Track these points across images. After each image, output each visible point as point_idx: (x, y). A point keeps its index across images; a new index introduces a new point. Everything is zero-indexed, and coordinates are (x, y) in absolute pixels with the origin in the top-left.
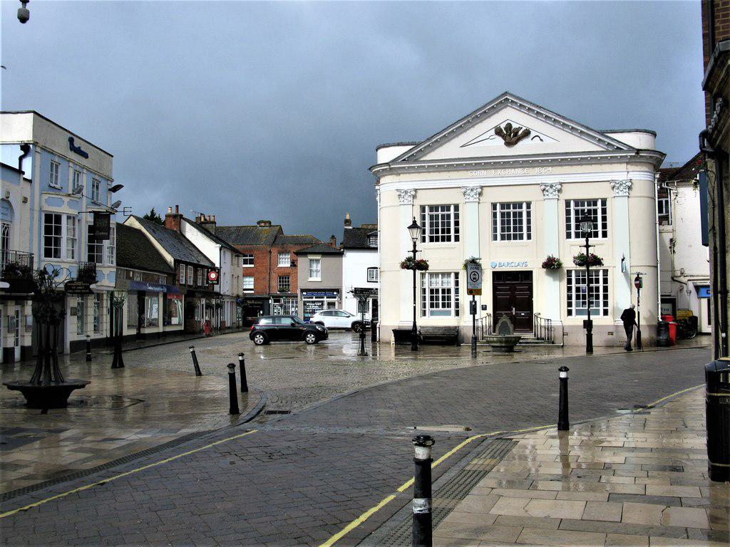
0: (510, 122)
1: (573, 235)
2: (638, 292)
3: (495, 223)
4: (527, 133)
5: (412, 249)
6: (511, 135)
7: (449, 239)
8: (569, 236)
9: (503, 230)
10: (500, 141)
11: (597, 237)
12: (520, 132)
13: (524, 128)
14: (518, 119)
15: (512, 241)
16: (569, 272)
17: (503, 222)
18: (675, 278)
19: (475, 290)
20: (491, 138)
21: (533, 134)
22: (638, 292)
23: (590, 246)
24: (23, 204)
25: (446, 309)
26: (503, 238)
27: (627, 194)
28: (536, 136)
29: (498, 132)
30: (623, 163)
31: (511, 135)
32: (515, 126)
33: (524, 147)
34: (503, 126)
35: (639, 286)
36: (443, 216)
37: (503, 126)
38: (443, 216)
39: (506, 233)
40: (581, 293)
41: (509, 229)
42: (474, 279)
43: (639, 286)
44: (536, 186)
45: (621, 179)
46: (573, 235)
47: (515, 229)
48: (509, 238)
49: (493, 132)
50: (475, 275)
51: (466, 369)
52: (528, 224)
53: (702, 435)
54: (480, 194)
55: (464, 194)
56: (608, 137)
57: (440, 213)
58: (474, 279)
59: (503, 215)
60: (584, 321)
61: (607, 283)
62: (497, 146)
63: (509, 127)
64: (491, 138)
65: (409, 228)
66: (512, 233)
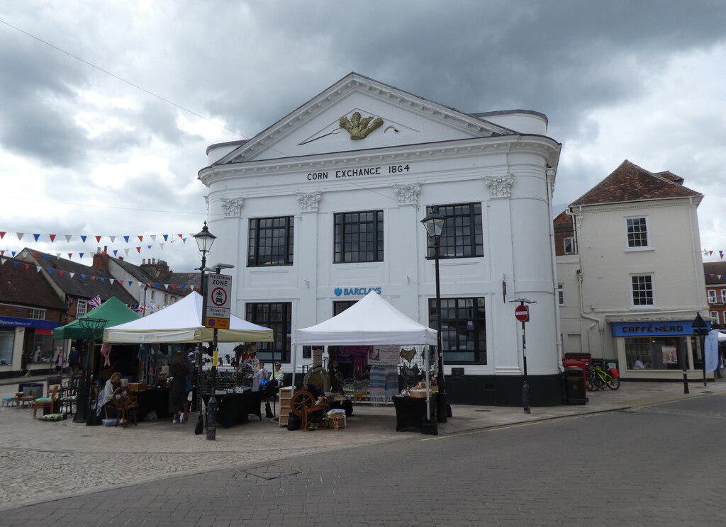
0: (356, 111)
2: (524, 328)
4: (379, 123)
6: (361, 127)
13: (375, 118)
14: (370, 108)
15: (653, 289)
19: (219, 320)
20: (335, 132)
21: (386, 124)
22: (524, 328)
24: (335, 290)
27: (317, 210)
28: (390, 127)
29: (344, 124)
30: (501, 153)
31: (361, 127)
32: (364, 116)
33: (375, 140)
34: (349, 117)
35: (523, 319)
37: (349, 117)
40: (645, 283)
42: (218, 300)
43: (523, 319)
44: (388, 189)
45: (499, 176)
49: (337, 125)
50: (219, 294)
51: (463, 334)
54: (319, 202)
55: (301, 201)
56: (484, 121)
58: (218, 300)
62: (342, 140)
64: (335, 132)
65: (196, 236)
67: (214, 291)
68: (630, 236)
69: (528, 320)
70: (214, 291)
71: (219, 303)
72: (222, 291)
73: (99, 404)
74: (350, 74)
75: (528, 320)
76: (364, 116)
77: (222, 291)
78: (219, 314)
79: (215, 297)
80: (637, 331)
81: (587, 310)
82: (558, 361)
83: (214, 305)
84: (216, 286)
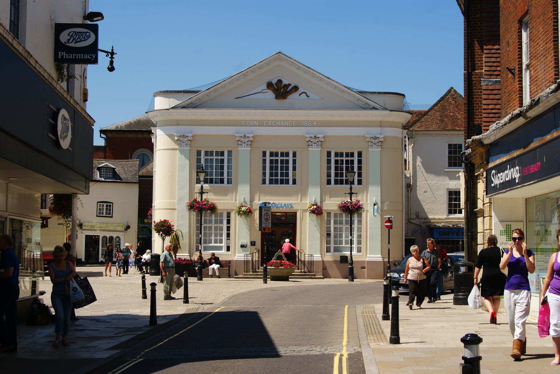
1: (333, 181)
3: (264, 168)
4: (296, 88)
5: (349, 192)
7: (287, 182)
8: (329, 182)
9: (271, 175)
10: (270, 95)
11: (288, 184)
12: (290, 88)
15: (279, 185)
16: (329, 214)
17: (271, 168)
18: (412, 221)
21: (301, 90)
23: (353, 193)
25: (218, 245)
26: (271, 182)
29: (269, 85)
36: (347, 161)
37: (274, 82)
38: (347, 161)
39: (339, 178)
41: (276, 175)
42: (267, 219)
46: (333, 181)
47: (282, 175)
48: (276, 182)
49: (265, 87)
50: (267, 215)
52: (265, 173)
53: (529, 347)
57: (344, 159)
59: (271, 161)
60: (81, 259)
61: (229, 224)
63: (280, 81)
66: (279, 178)
67: (265, 214)
68: (450, 158)
69: (392, 228)
70: (265, 214)
71: (267, 220)
72: (267, 214)
73: (539, 163)
74: (278, 53)
75: (392, 228)
76: (285, 82)
77: (267, 214)
78: (267, 226)
79: (265, 217)
80: (449, 235)
81: (413, 216)
82: (403, 253)
83: (265, 221)
84: (265, 212)
